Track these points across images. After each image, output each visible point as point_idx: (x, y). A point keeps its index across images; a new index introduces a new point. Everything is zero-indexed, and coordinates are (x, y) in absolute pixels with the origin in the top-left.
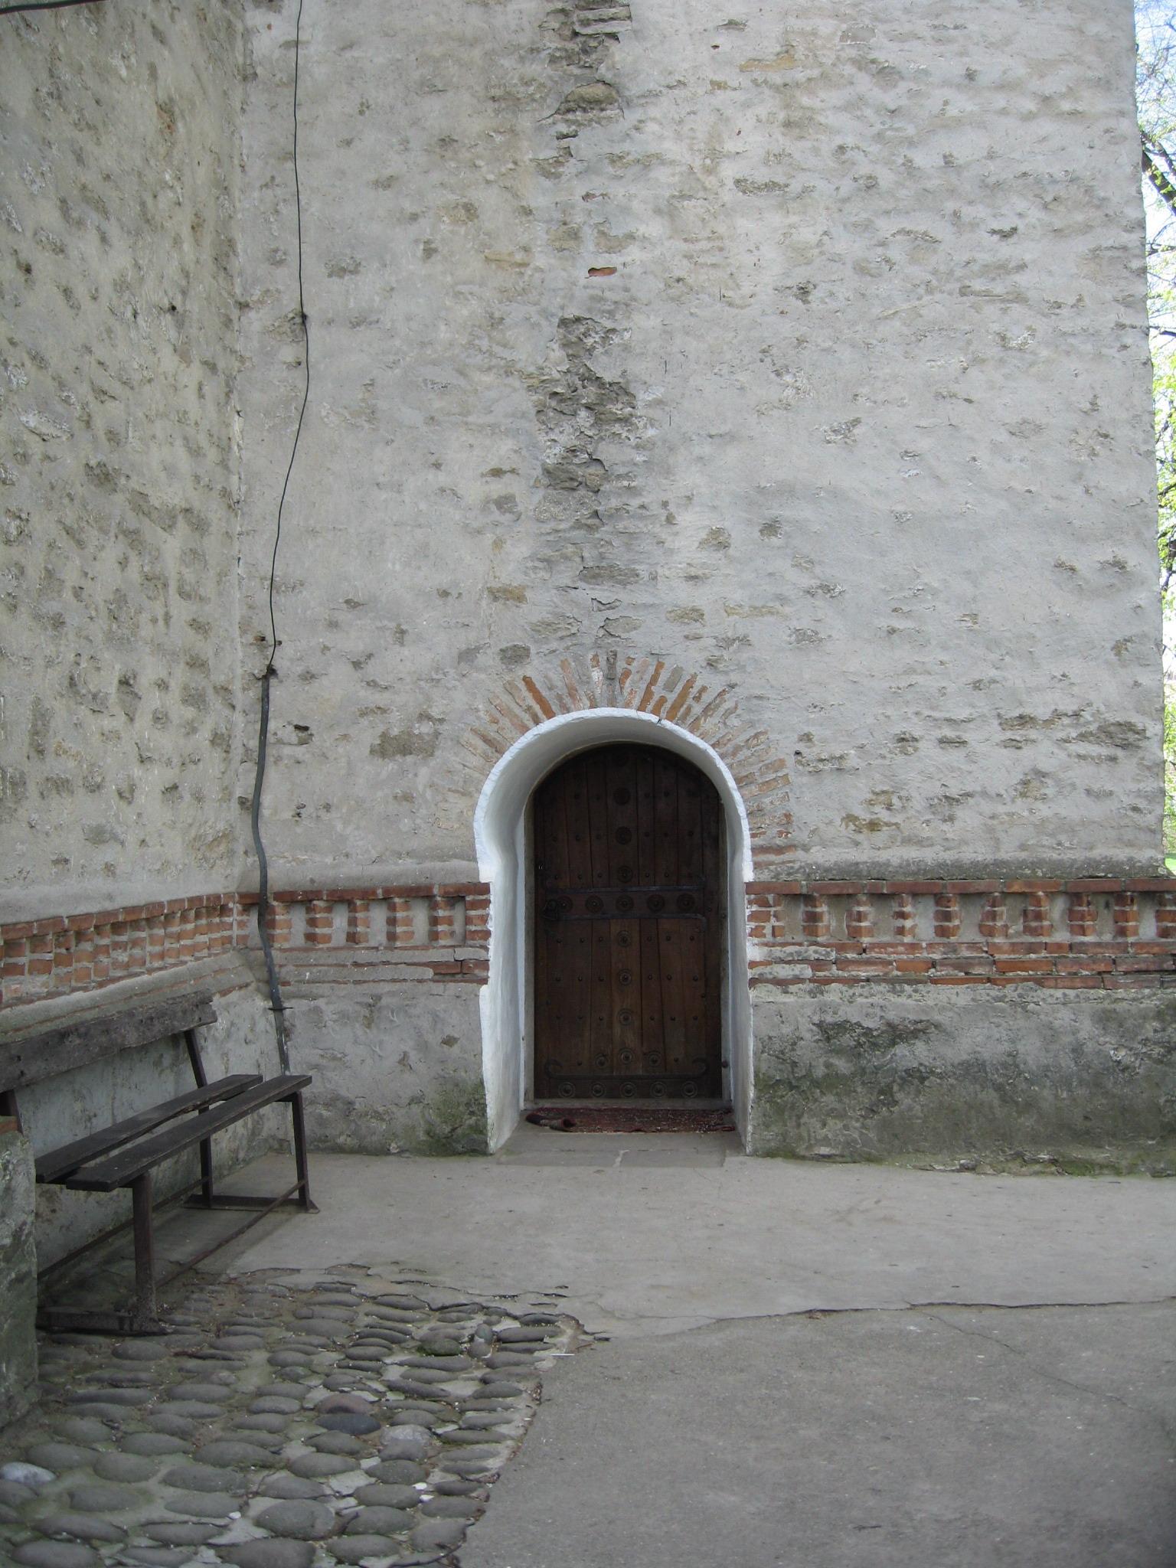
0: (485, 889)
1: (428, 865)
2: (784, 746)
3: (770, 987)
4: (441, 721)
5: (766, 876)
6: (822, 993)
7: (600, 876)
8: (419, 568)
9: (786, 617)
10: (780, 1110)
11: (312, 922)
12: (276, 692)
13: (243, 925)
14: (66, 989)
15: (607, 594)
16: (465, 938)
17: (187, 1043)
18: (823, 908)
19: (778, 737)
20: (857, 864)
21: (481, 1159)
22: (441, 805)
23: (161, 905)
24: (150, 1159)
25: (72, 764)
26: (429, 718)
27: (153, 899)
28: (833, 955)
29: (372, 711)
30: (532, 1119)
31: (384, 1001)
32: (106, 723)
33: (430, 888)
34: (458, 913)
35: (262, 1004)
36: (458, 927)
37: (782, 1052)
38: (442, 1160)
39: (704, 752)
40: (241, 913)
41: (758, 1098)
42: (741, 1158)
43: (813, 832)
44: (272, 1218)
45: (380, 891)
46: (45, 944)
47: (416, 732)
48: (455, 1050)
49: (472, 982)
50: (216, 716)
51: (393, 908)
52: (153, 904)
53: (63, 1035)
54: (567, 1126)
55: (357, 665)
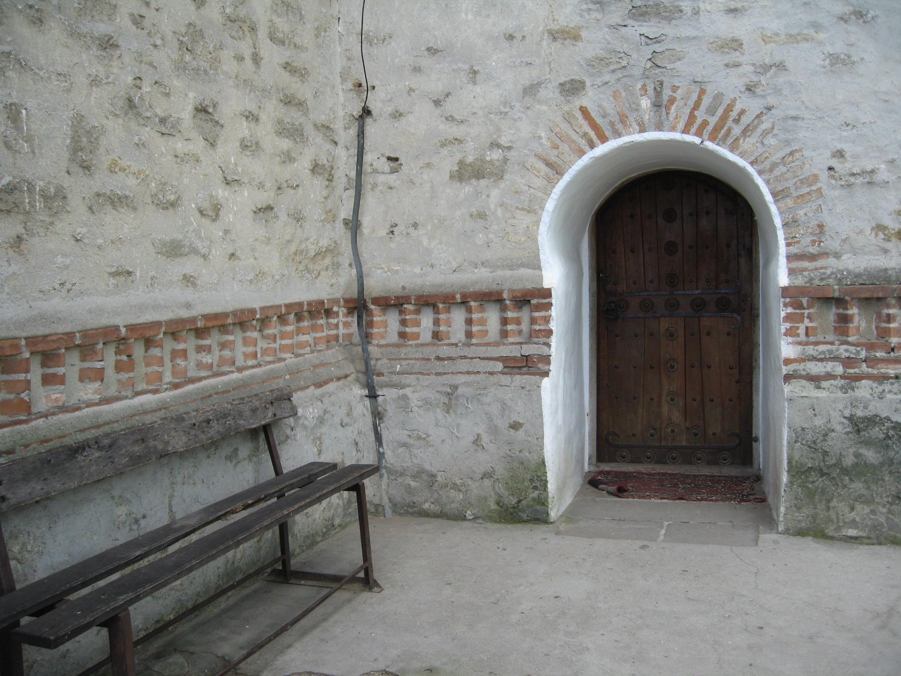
0: (547, 293)
1: (500, 273)
2: (817, 161)
3: (804, 382)
4: (509, 148)
5: (800, 281)
6: (853, 389)
7: (651, 282)
8: (488, 16)
9: (821, 43)
10: (811, 494)
11: (403, 323)
12: (371, 128)
13: (345, 325)
14: (129, 394)
15: (654, 29)
16: (531, 336)
17: (265, 435)
18: (853, 311)
19: (813, 154)
20: (886, 270)
21: (543, 527)
22: (510, 221)
23: (253, 311)
24: (131, 595)
25: (132, 181)
26: (499, 146)
27: (244, 306)
28: (863, 354)
29: (450, 142)
30: (593, 482)
31: (460, 391)
32: (180, 146)
33: (500, 293)
34: (525, 315)
35: (359, 392)
36: (525, 326)
37: (814, 442)
38: (509, 526)
39: (742, 170)
40: (346, 315)
41: (791, 483)
42: (774, 536)
43: (845, 241)
44: (340, 596)
45: (458, 296)
46: (95, 353)
47: (488, 159)
48: (521, 434)
49: (534, 374)
50: (316, 148)
51: (469, 310)
52: (242, 311)
53: (75, 450)
54: (621, 492)
55: (437, 103)
